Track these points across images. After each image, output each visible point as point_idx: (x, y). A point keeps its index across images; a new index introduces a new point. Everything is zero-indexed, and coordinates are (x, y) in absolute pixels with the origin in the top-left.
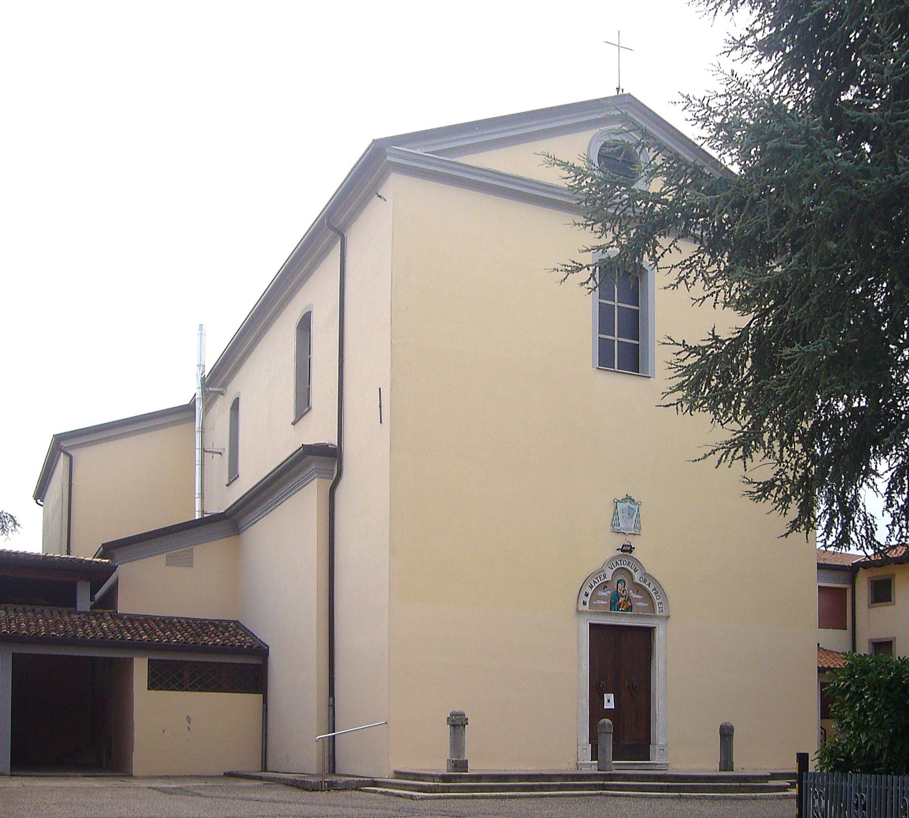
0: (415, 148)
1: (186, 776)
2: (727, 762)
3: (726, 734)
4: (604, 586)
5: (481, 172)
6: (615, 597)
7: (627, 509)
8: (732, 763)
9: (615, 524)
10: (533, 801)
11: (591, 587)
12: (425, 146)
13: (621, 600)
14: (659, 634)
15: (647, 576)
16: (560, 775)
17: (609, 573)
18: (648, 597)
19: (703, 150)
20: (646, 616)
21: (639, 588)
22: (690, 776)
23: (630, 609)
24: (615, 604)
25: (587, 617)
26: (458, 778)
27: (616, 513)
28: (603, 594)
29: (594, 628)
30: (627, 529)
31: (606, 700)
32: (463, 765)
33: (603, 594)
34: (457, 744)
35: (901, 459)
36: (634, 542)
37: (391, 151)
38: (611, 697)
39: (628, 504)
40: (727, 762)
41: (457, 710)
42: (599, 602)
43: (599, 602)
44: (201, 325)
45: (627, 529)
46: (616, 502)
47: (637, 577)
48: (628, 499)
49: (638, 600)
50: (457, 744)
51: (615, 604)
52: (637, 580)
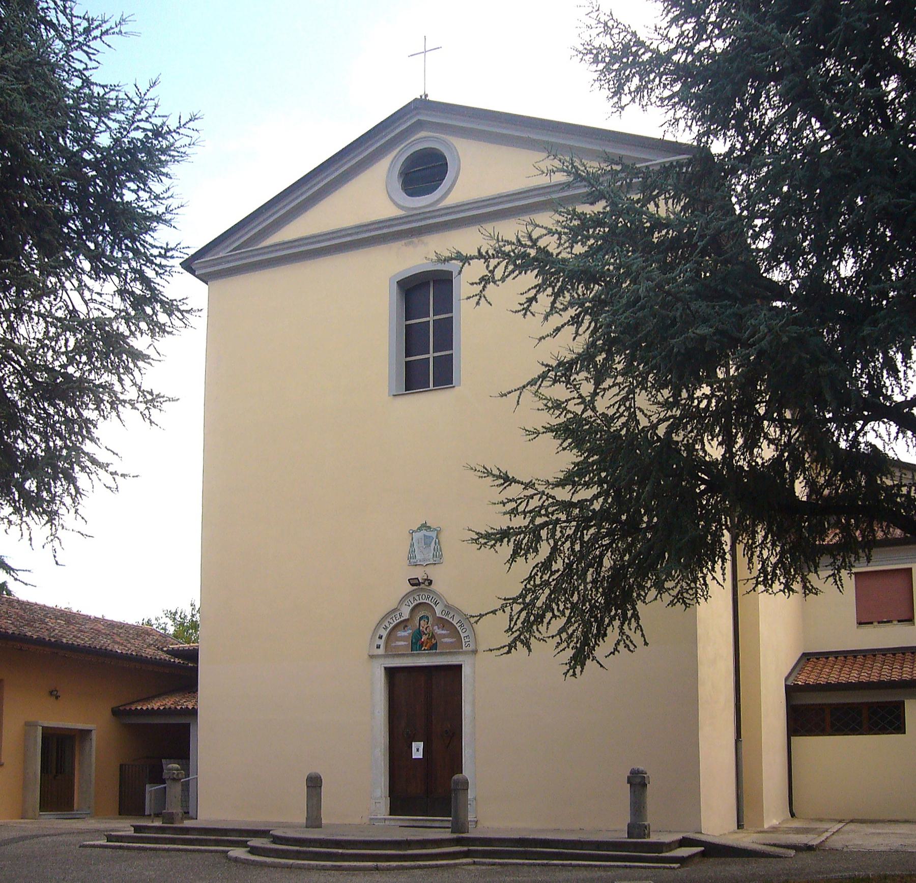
0: (218, 253)
1: (890, 821)
2: (314, 820)
3: (314, 783)
4: (404, 624)
5: (270, 249)
6: (418, 634)
9: (411, 555)
10: (120, 852)
11: (386, 628)
12: (224, 249)
13: (424, 638)
14: (466, 672)
15: (449, 608)
17: (406, 612)
18: (455, 632)
20: (450, 653)
21: (443, 623)
23: (434, 647)
24: (417, 643)
26: (636, 848)
27: (412, 545)
29: (391, 672)
30: (424, 560)
31: (414, 749)
34: (638, 806)
35: (86, 399)
36: (433, 573)
37: (198, 266)
38: (421, 745)
39: (424, 532)
40: (314, 820)
45: (424, 560)
46: (439, 532)
47: (438, 610)
48: (425, 526)
49: (444, 636)
50: (638, 806)
51: (417, 643)
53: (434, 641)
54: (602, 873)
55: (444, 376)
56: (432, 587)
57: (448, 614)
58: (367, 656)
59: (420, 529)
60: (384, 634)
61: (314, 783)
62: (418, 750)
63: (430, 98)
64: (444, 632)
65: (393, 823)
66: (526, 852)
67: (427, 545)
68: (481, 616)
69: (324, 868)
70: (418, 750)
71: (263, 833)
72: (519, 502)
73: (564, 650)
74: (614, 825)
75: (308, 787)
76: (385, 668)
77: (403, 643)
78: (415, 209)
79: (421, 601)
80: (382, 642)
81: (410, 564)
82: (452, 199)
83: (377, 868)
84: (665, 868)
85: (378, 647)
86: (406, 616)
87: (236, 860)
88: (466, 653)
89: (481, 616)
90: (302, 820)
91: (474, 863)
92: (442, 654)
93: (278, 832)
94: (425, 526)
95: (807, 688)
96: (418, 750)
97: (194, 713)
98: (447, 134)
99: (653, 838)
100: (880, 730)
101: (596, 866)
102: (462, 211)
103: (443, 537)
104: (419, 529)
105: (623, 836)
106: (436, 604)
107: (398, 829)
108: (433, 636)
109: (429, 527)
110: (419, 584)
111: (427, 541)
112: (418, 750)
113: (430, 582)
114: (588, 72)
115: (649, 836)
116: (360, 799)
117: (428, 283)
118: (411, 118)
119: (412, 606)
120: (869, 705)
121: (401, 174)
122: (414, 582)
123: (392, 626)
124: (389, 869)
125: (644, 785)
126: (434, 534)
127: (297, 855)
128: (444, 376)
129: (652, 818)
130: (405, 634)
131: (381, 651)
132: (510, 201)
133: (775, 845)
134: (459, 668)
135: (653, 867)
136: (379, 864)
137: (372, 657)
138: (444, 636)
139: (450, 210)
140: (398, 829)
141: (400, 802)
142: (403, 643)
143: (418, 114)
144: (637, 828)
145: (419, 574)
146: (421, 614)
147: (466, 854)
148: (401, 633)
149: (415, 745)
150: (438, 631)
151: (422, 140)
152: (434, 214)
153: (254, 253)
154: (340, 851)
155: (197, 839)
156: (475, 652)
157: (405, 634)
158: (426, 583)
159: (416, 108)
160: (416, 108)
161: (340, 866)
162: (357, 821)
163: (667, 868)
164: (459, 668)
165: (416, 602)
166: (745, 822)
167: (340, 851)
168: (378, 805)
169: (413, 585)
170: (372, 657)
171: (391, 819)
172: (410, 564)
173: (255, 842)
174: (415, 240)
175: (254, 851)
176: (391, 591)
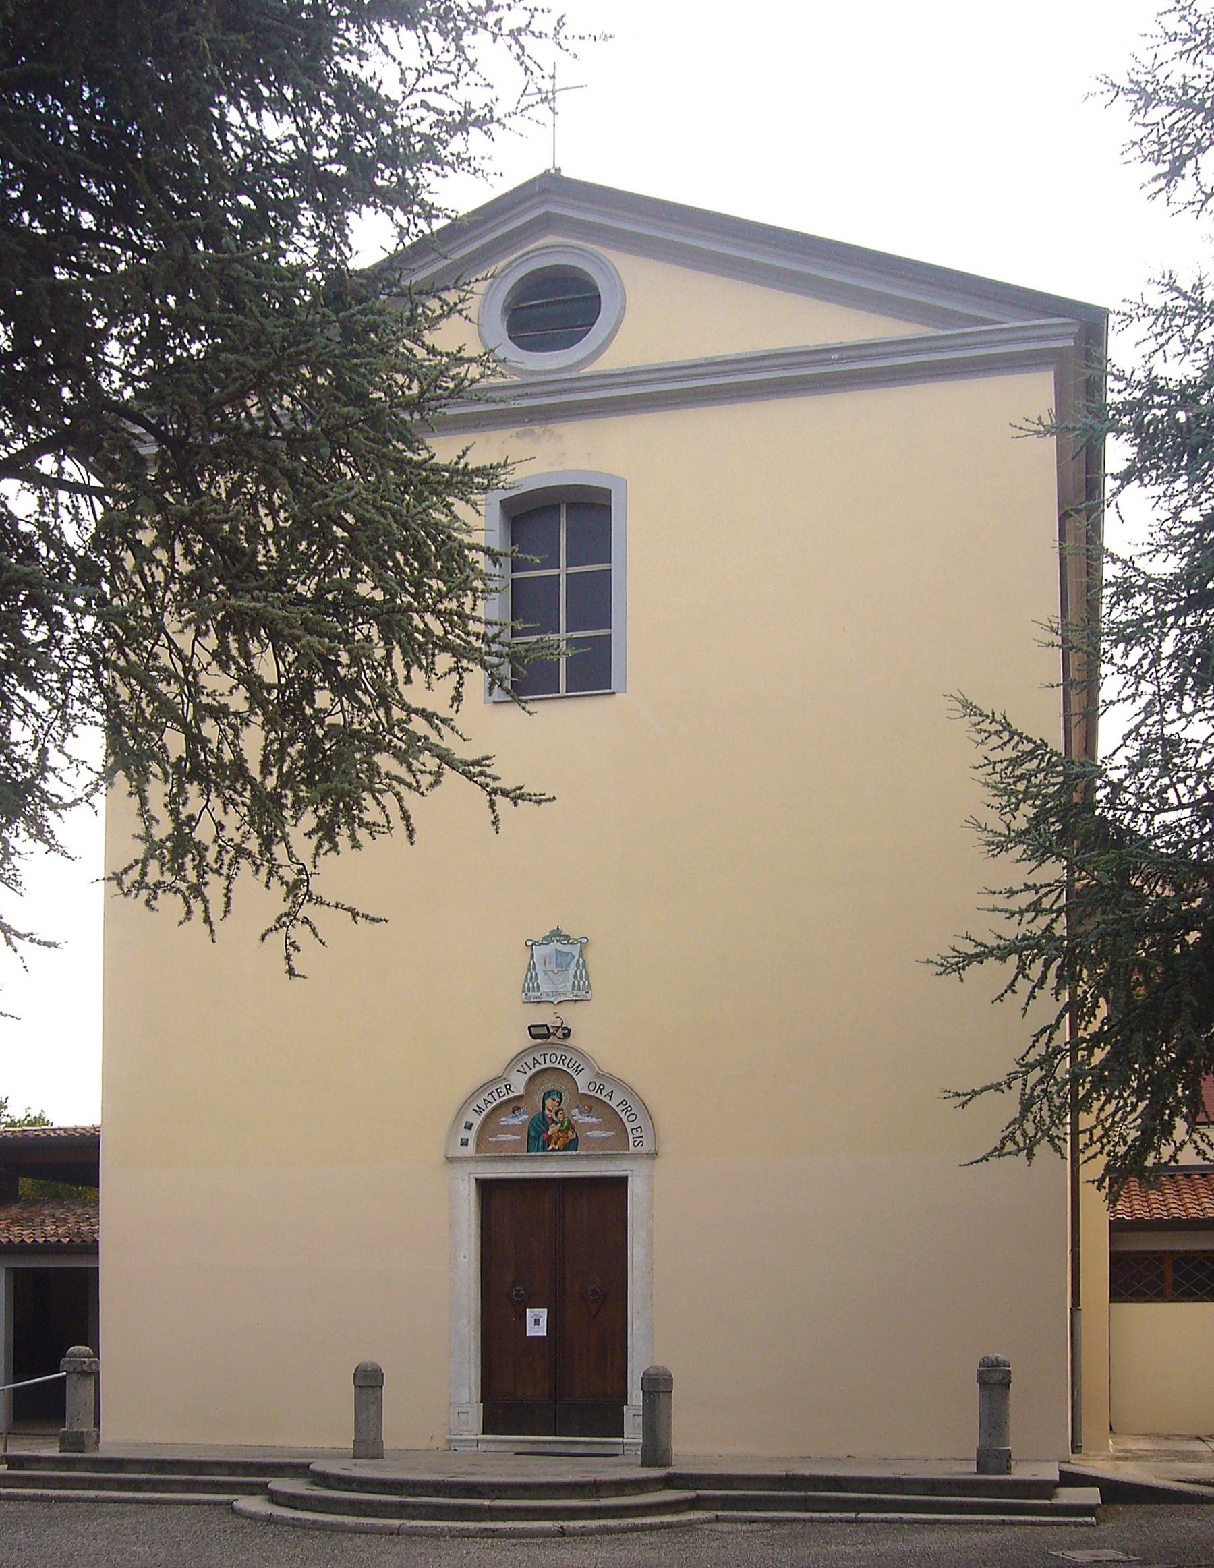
2: (368, 1443)
3: (369, 1382)
4: (514, 1105)
7: (563, 952)
8: (668, 1450)
11: (479, 1111)
13: (552, 1129)
14: (635, 1189)
16: (219, 1464)
17: (518, 1084)
18: (613, 1120)
19: (439, 231)
21: (591, 1104)
22: (252, 1465)
23: (572, 1144)
24: (538, 1138)
25: (470, 1168)
26: (992, 1490)
27: (532, 967)
28: (512, 1121)
29: (486, 1188)
32: (1004, 1461)
33: (512, 1121)
34: (994, 1419)
36: (572, 1016)
38: (543, 1313)
40: (368, 1443)
41: (993, 1355)
42: (502, 1137)
43: (502, 1137)
44: (429, 688)
45: (556, 993)
46: (584, 945)
47: (582, 1081)
49: (592, 1127)
50: (994, 1419)
51: (538, 1138)
52: (583, 1088)
54: (975, 1537)
55: (593, 672)
56: (570, 1042)
59: (547, 940)
60: (477, 1120)
61: (369, 1382)
62: (537, 1322)
63: (564, 173)
64: (590, 1120)
65: (493, 1447)
66: (806, 1499)
67: (563, 968)
68: (974, 1093)
69: (464, 1534)
70: (537, 1322)
71: (299, 1470)
72: (1043, 891)
73: (1094, 1156)
74: (949, 1453)
77: (509, 1137)
78: (532, 373)
79: (549, 1065)
80: (471, 1135)
81: (527, 1001)
82: (609, 362)
83: (563, 1533)
84: (1076, 1524)
85: (464, 1143)
86: (519, 1088)
87: (252, 1517)
89: (974, 1093)
90: (348, 1443)
91: (717, 1519)
93: (318, 1466)
94: (557, 935)
95: (1138, 1225)
96: (537, 1323)
97: (92, 1249)
98: (607, 246)
99: (1020, 1472)
100: (1182, 1294)
101: (925, 1522)
102: (634, 384)
103: (592, 955)
104: (545, 938)
105: (967, 1470)
106: (578, 1071)
107: (505, 1460)
108: (570, 1126)
109: (567, 937)
110: (547, 1036)
111: (562, 961)
112: (537, 1323)
113: (567, 1034)
114: (1121, 122)
115: (1008, 1470)
116: (438, 1411)
117: (557, 508)
118: (534, 207)
119: (530, 1073)
120: (1188, 1256)
121: (506, 309)
122: (539, 1033)
123: (490, 1107)
124: (582, 1533)
125: (1007, 1385)
126: (575, 950)
127: (401, 1511)
128: (593, 672)
129: (1014, 1444)
131: (470, 1150)
132: (903, 354)
133: (1197, 1482)
134: (621, 1183)
135: (1053, 1523)
136: (565, 1524)
137: (451, 1160)
138: (592, 1127)
139: (628, 376)
140: (505, 1460)
141: (503, 1409)
142: (509, 1137)
143: (546, 202)
144: (993, 1456)
145: (543, 1015)
146: (549, 1086)
147: (694, 1504)
148: (508, 1120)
151: (551, 251)
152: (577, 385)
153: (969, 340)
154: (487, 1503)
155: (148, 1481)
156: (653, 1155)
158: (560, 1033)
159: (544, 191)
160: (544, 191)
162: (423, 1444)
163: (1081, 1525)
164: (621, 1183)
165: (538, 1067)
166: (1084, 1441)
167: (487, 1503)
169: (534, 1037)
170: (451, 1160)
171: (487, 1441)
172: (527, 1001)
173: (278, 1484)
174: (537, 429)
175: (276, 1498)
176: (493, 1044)
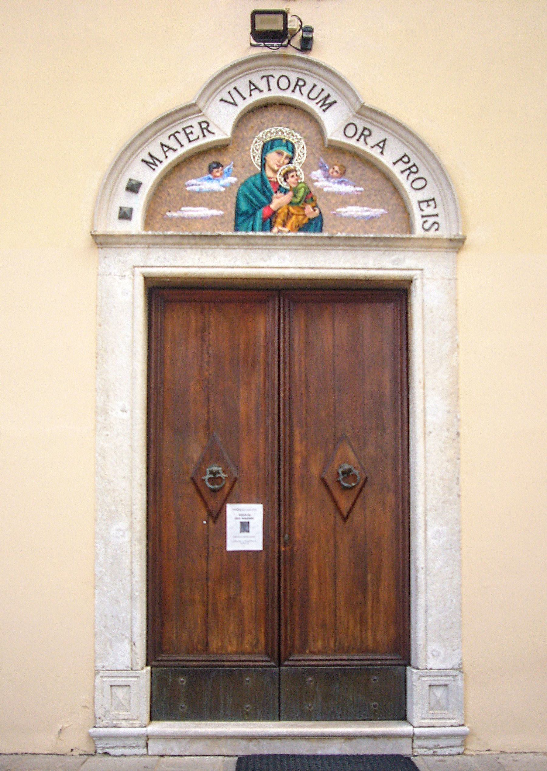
4: (211, 157)
11: (151, 162)
13: (279, 201)
14: (424, 303)
17: (222, 121)
23: (315, 224)
29: (162, 294)
38: (255, 513)
49: (345, 200)
53: (310, 212)
57: (365, 134)
58: (85, 239)
60: (149, 178)
64: (349, 189)
75: (280, 719)
76: (146, 279)
79: (275, 93)
80: (138, 203)
85: (125, 215)
88: (428, 245)
92: (334, 243)
106: (327, 104)
108: (309, 197)
112: (245, 527)
119: (243, 105)
123: (172, 156)
130: (215, 186)
134: (396, 294)
137: (101, 241)
138: (345, 200)
146: (272, 132)
149: (234, 513)
150: (322, 183)
157: (215, 186)
161: (275, 354)
164: (396, 294)
165: (257, 97)
168: (120, 693)
170: (101, 241)
